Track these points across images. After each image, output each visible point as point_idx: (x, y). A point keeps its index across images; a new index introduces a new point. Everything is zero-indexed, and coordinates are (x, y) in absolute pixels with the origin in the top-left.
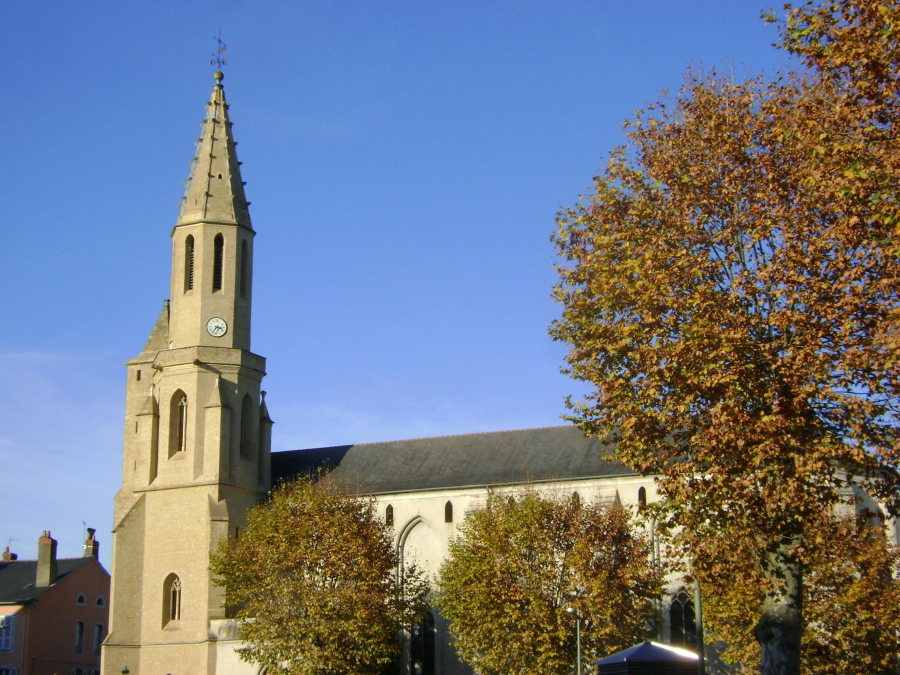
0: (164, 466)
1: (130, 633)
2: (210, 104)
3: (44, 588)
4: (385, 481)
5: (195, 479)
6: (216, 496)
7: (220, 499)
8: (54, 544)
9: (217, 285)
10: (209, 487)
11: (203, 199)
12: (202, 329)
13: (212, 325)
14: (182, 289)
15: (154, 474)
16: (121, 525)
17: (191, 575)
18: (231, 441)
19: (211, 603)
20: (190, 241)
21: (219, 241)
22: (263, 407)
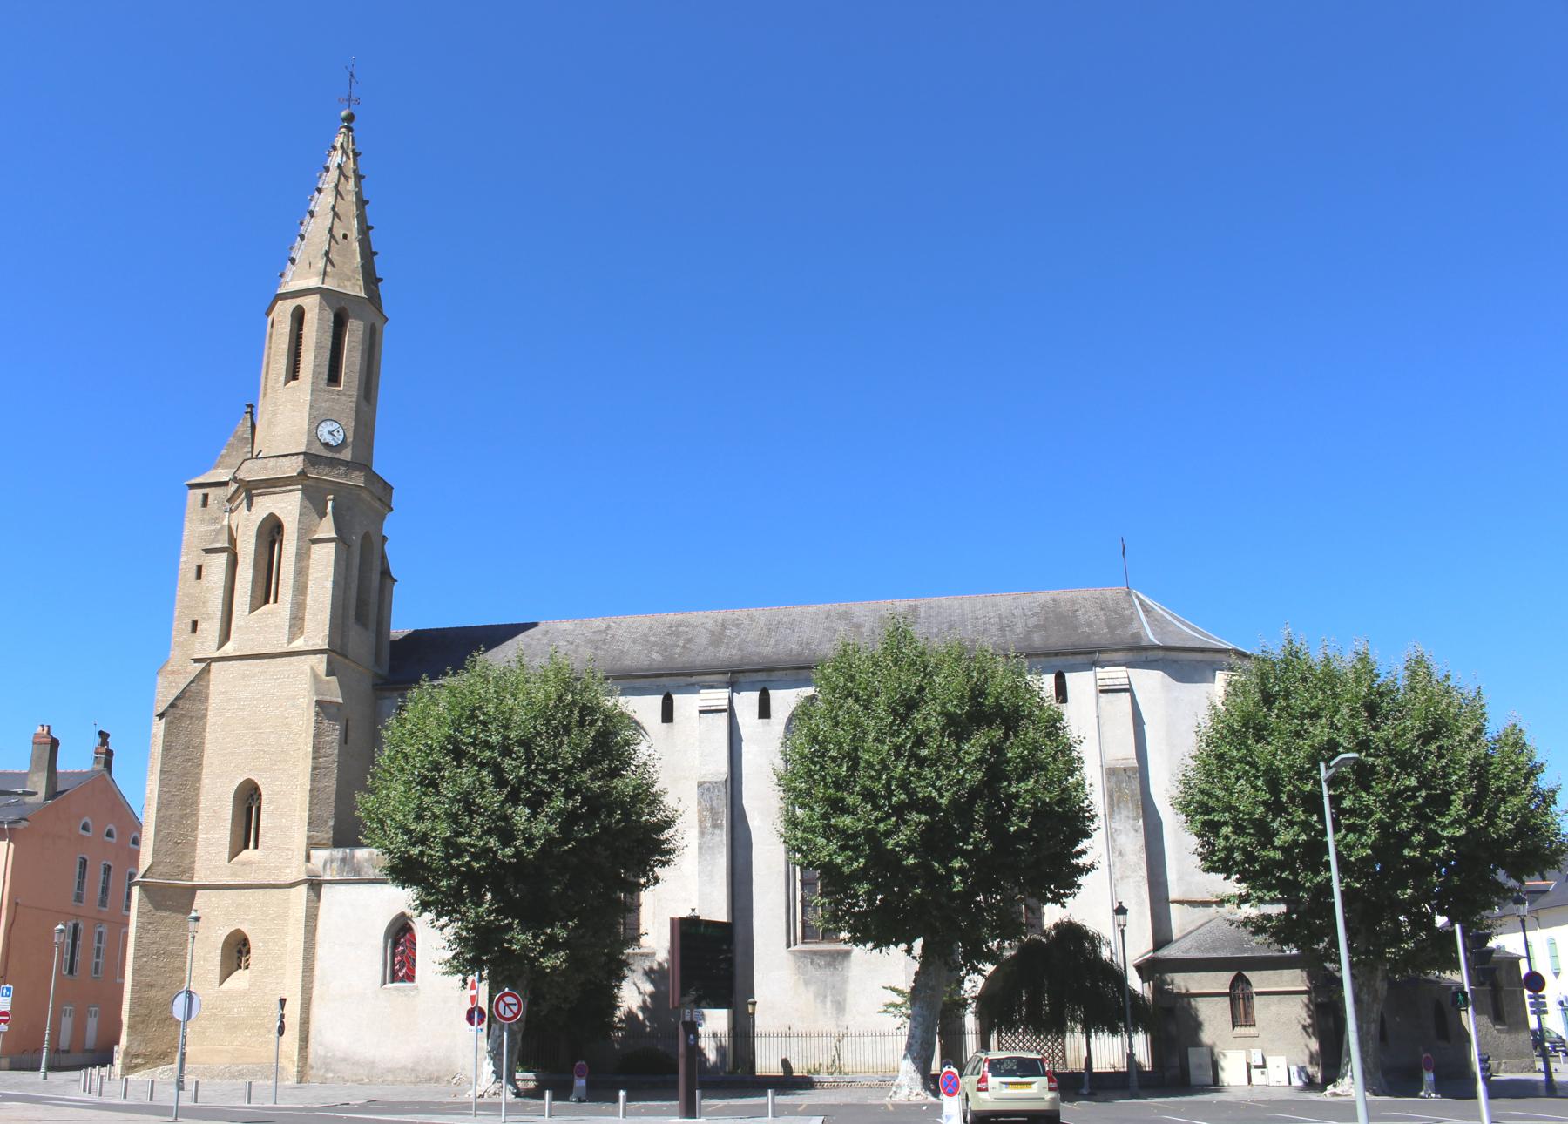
0: (242, 623)
2: (334, 148)
3: (38, 804)
8: (55, 744)
9: (334, 377)
11: (321, 263)
12: (309, 431)
14: (283, 379)
15: (225, 636)
16: (172, 705)
19: (312, 823)
20: (299, 316)
22: (383, 557)
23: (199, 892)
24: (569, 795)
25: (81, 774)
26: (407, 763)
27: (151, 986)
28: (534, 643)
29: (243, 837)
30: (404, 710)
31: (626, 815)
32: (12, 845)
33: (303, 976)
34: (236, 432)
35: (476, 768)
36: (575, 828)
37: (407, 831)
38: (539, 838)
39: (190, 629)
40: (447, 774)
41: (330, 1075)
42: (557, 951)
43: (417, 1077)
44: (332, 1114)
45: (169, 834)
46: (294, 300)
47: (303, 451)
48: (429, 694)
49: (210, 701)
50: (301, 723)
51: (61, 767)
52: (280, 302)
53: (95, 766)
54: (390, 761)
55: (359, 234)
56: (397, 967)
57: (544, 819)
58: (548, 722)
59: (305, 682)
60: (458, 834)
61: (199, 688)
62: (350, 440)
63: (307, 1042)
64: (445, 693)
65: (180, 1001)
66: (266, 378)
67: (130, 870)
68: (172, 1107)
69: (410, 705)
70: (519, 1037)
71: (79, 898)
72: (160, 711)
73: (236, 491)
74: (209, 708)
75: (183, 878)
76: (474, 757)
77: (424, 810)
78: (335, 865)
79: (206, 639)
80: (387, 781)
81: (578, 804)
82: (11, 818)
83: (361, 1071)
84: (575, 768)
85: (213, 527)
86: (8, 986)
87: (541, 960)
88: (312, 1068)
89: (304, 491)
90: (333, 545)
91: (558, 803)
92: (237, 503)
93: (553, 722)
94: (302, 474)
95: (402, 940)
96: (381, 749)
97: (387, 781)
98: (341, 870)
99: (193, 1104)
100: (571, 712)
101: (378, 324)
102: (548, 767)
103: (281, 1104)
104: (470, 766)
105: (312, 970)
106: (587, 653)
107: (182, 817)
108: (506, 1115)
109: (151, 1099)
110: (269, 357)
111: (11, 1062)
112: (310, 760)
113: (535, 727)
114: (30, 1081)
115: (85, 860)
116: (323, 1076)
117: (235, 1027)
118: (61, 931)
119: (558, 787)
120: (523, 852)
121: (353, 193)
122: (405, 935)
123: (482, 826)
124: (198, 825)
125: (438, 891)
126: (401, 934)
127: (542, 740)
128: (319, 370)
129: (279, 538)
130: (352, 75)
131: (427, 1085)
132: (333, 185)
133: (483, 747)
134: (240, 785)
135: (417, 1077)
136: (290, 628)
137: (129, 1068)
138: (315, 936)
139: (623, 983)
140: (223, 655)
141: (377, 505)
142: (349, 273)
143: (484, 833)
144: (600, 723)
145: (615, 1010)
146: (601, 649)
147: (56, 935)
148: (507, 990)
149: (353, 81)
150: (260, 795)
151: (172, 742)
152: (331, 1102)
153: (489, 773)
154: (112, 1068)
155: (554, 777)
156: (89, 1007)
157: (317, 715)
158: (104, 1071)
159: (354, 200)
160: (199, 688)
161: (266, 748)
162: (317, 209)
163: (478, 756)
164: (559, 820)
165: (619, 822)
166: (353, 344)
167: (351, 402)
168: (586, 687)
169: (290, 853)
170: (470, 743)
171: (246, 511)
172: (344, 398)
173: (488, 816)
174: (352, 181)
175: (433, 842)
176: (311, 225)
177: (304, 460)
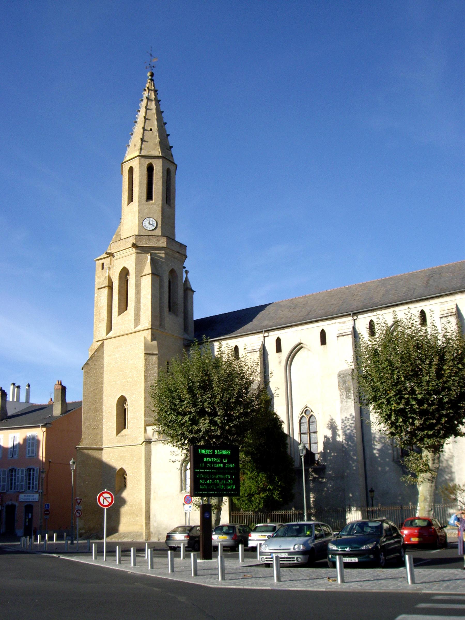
1: (95, 440)
4: (275, 323)
6: (149, 338)
7: (152, 340)
8: (64, 389)
9: (150, 196)
10: (145, 331)
13: (146, 222)
15: (109, 328)
16: (87, 364)
17: (134, 396)
18: (161, 299)
20: (131, 170)
21: (150, 169)
63: (149, 521)
130: (151, 55)
134: (119, 398)
148: (106, 490)
161: (128, 380)
166: (158, 179)
167: (159, 207)
172: (155, 206)
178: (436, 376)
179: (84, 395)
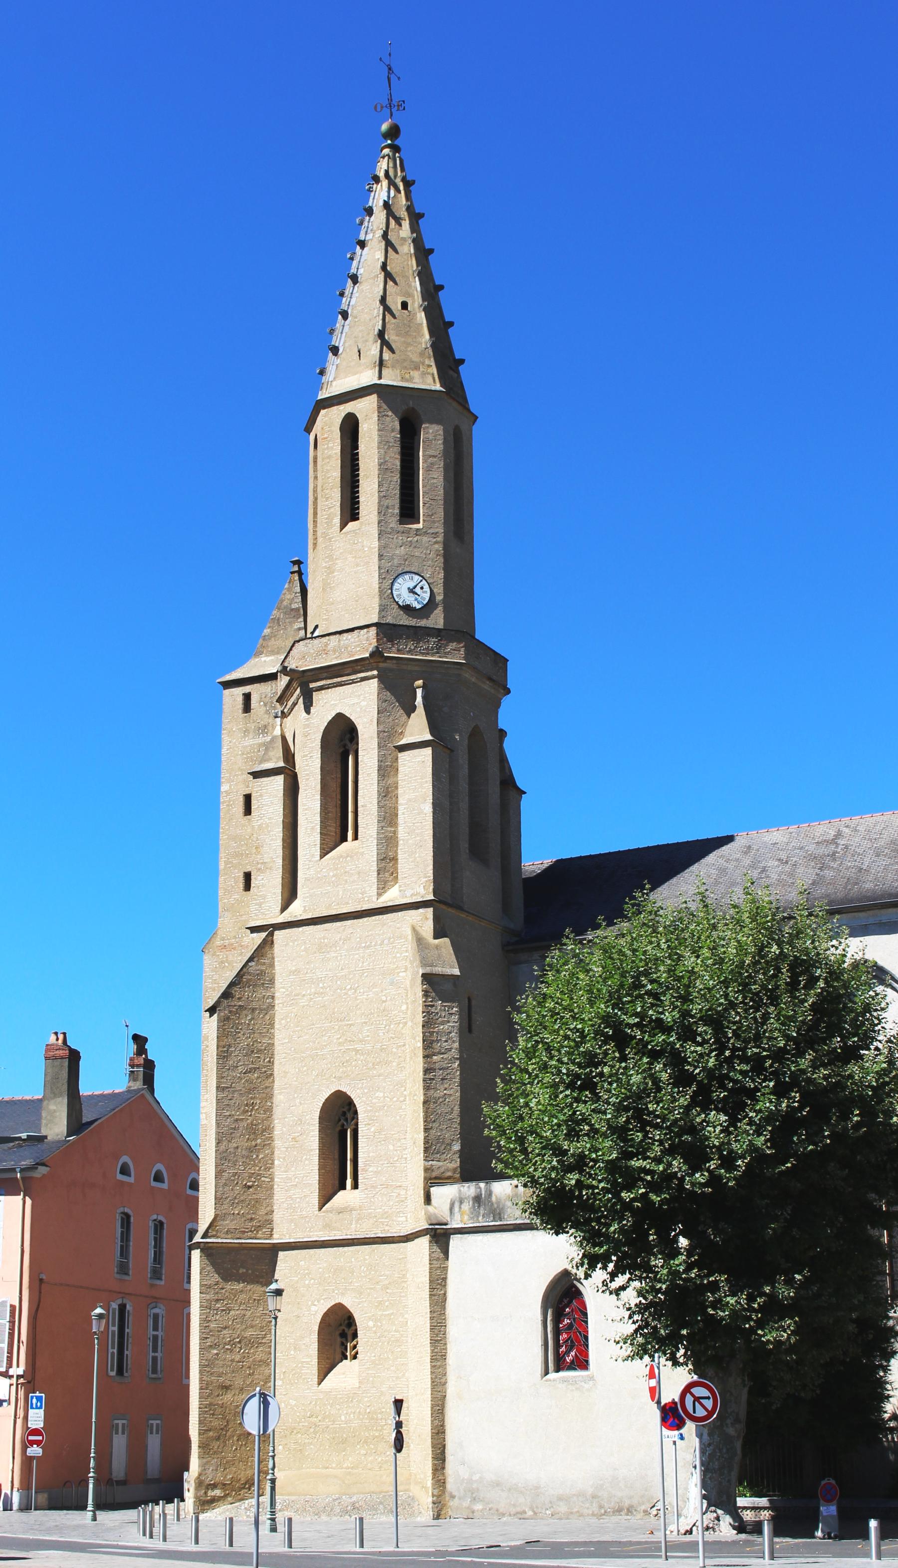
0: (312, 872)
2: (377, 179)
3: (59, 1142)
5: (380, 893)
7: (437, 936)
8: (74, 1057)
12: (381, 592)
14: (337, 520)
16: (226, 995)
20: (350, 427)
22: (503, 760)
23: (281, 1254)
24: (781, 1091)
25: (113, 1096)
26: (551, 1058)
27: (226, 1388)
28: (731, 866)
29: (337, 1173)
30: (542, 982)
31: (869, 1113)
32: (29, 1201)
33: (433, 1367)
34: (282, 601)
35: (645, 1060)
36: (795, 1139)
37: (559, 1152)
38: (743, 1157)
39: (241, 884)
40: (606, 1070)
41: (478, 1507)
42: (782, 1318)
43: (601, 1507)
44: (469, 1559)
45: (235, 1174)
46: (342, 407)
47: (375, 620)
48: (575, 956)
49: (278, 984)
50: (404, 1007)
51: (85, 1089)
52: (323, 412)
53: (132, 1084)
54: (527, 1056)
55: (424, 300)
56: (563, 1349)
57: (748, 1128)
58: (745, 986)
59: (407, 951)
60: (629, 1156)
61: (259, 967)
62: (439, 598)
63: (444, 1460)
64: (598, 955)
65: (252, 1408)
66: (315, 522)
67: (189, 1226)
68: (252, 1553)
69: (550, 975)
70: (738, 1445)
71: (123, 1269)
72: (211, 1003)
73: (288, 686)
74: (276, 995)
75: (258, 1236)
76: (643, 1043)
77: (578, 1123)
78: (466, 1207)
79: (264, 897)
80: (525, 1084)
81: (796, 1104)
82: (25, 1163)
83: (521, 1500)
84: (788, 1052)
85: (261, 739)
86: (38, 1394)
87: (760, 1332)
88: (453, 1497)
89: (381, 678)
90: (428, 751)
91: (767, 1104)
92: (290, 703)
93: (753, 987)
94: (377, 654)
95: (567, 1309)
96: (514, 1040)
97: (525, 1084)
98: (475, 1214)
99: (286, 1549)
100: (778, 970)
101: (464, 428)
102: (749, 1052)
103: (404, 1548)
104: (637, 1057)
105: (444, 1357)
106: (805, 876)
107: (250, 1150)
108: (704, 1557)
109: (231, 1545)
110: (315, 491)
111: (50, 1499)
112: (420, 1059)
113: (726, 996)
114: (75, 1523)
115: (128, 1216)
116: (468, 1508)
117: (344, 1441)
118: (100, 1316)
119: (764, 1081)
120: (720, 1177)
121: (410, 241)
122: (570, 1302)
123: (661, 1142)
124: (273, 1161)
125: (608, 1238)
126: (566, 1301)
127: (738, 1013)
128: (386, 502)
129: (351, 747)
130: (390, 69)
131: (615, 1519)
132: (380, 233)
133: (653, 1029)
135: (601, 1507)
136: (379, 874)
137: (204, 1504)
138: (445, 1308)
139: (893, 1361)
140: (290, 920)
141: (487, 686)
142: (416, 358)
143: (665, 1152)
144: (821, 984)
145: (883, 1402)
146: (829, 868)
147: (94, 1322)
149: (392, 77)
150: (356, 1112)
151: (230, 1046)
152: (475, 1543)
153: (665, 1065)
154: (181, 1504)
155: (757, 1065)
156: (148, 1420)
157: (426, 994)
158: (170, 1508)
159: (412, 251)
160: (259, 967)
161: (358, 1046)
162: (361, 271)
163: (648, 1043)
164: (770, 1129)
165: (857, 1126)
167: (436, 543)
168: (799, 932)
169: (403, 1192)
170: (635, 1025)
171: (304, 714)
172: (425, 539)
173: (667, 1128)
174: (406, 224)
175: (592, 1167)
176: (355, 295)
177: (377, 634)
178: (562, 936)
179: (217, 1088)
